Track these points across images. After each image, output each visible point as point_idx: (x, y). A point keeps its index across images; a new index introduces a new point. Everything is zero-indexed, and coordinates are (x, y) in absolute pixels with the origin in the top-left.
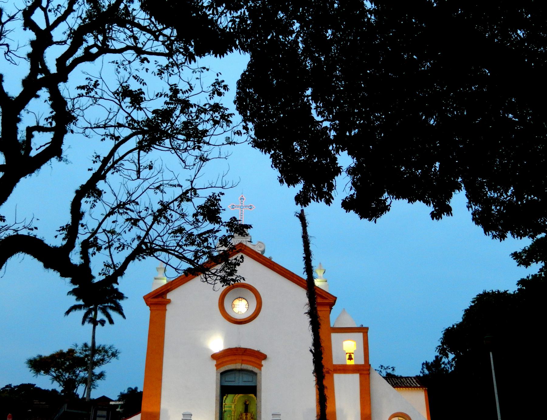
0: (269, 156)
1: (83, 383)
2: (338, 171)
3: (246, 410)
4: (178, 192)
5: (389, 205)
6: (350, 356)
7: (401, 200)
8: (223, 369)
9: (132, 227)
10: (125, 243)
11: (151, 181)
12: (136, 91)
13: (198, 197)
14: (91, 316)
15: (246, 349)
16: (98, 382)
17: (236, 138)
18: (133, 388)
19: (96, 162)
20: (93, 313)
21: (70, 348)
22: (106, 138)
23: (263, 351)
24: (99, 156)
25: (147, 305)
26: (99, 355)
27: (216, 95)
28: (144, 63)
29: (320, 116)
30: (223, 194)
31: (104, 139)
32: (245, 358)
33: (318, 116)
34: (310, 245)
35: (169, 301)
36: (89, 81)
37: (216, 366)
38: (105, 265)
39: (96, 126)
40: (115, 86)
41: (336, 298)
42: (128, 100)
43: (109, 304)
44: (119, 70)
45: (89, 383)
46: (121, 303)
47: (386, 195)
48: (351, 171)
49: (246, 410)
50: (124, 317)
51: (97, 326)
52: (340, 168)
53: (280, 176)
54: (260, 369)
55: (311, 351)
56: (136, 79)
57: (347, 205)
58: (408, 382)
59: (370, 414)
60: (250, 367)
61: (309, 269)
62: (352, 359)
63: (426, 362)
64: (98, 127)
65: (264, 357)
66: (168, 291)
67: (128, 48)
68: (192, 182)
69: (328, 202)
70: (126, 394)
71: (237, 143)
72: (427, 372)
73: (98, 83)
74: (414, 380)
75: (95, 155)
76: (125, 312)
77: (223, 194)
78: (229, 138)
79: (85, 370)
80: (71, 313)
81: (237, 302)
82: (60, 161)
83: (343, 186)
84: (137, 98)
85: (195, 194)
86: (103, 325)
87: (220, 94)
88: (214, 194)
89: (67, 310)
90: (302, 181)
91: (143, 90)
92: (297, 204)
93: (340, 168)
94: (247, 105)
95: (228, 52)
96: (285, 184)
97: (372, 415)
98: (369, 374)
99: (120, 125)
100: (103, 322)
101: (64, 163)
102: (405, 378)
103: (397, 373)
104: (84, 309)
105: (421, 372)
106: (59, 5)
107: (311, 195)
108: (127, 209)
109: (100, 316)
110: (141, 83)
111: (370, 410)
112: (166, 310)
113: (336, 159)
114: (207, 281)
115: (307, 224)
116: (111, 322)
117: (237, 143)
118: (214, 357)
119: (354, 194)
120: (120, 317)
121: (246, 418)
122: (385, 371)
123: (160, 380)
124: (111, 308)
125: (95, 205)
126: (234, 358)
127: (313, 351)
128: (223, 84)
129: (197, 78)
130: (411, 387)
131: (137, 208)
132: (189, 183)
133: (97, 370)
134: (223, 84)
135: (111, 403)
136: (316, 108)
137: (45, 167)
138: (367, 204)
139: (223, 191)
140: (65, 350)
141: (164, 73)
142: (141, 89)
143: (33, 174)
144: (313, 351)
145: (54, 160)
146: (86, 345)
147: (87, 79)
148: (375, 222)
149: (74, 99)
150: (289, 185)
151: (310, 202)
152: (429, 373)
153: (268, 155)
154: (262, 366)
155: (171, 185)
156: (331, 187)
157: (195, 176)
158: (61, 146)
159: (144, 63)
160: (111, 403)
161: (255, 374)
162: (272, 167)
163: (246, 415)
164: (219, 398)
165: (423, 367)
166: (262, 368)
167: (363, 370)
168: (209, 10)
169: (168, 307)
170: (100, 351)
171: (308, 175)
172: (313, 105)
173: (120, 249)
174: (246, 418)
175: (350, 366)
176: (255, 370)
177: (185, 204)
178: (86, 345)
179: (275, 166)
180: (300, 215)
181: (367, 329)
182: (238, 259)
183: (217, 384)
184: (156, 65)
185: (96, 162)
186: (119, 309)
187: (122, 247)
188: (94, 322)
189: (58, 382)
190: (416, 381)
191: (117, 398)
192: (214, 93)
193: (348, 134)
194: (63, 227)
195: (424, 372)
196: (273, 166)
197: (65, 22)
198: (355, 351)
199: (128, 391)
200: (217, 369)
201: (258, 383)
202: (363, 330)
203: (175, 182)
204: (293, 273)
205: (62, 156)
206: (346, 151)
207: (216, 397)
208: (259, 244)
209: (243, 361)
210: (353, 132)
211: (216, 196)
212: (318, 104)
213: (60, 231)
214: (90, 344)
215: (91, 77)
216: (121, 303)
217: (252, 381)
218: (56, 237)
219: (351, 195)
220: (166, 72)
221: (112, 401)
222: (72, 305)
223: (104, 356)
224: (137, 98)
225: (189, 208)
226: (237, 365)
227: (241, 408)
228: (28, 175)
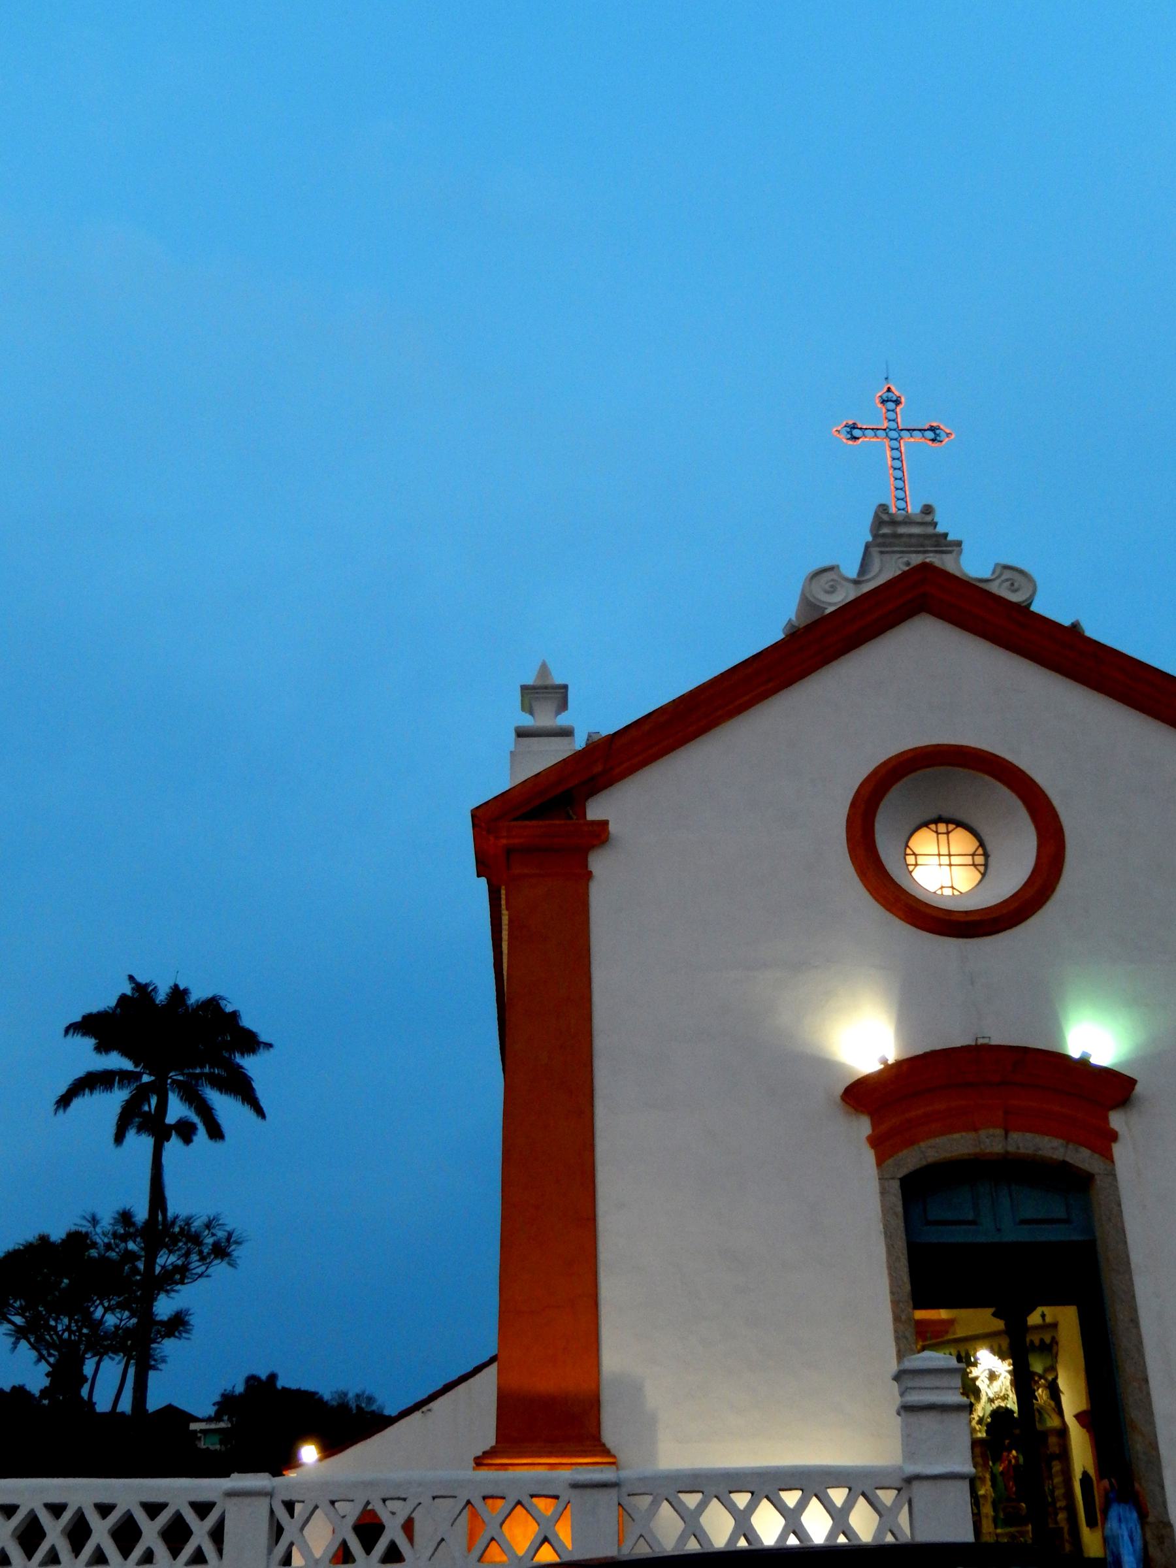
1: (116, 1352)
8: (911, 1159)
16: (168, 1347)
20: (154, 1101)
21: (74, 1228)
26: (171, 1252)
35: (599, 834)
37: (876, 1142)
43: (207, 1070)
45: (139, 1347)
46: (250, 1064)
50: (260, 1112)
51: (168, 1145)
54: (1108, 1156)
60: (1051, 1147)
79: (122, 1306)
80: (77, 1103)
89: (62, 1089)
104: (121, 1087)
109: (177, 1109)
112: (589, 875)
116: (216, 1132)
118: (862, 1095)
120: (247, 1112)
123: (585, 1220)
133: (164, 1307)
135: (194, 1426)
140: (57, 1234)
146: (125, 1217)
154: (1114, 1136)
160: (194, 1426)
166: (1117, 1149)
169: (600, 864)
170: (175, 1239)
176: (1083, 1158)
178: (125, 1217)
183: (888, 1235)
186: (242, 1088)
188: (159, 1131)
189: (33, 1347)
191: (211, 1411)
200: (880, 1162)
208: (1007, 574)
214: (141, 1214)
216: (250, 1064)
217: (1067, 1221)
221: (196, 1420)
222: (80, 1073)
223: (187, 1254)
226: (983, 1133)
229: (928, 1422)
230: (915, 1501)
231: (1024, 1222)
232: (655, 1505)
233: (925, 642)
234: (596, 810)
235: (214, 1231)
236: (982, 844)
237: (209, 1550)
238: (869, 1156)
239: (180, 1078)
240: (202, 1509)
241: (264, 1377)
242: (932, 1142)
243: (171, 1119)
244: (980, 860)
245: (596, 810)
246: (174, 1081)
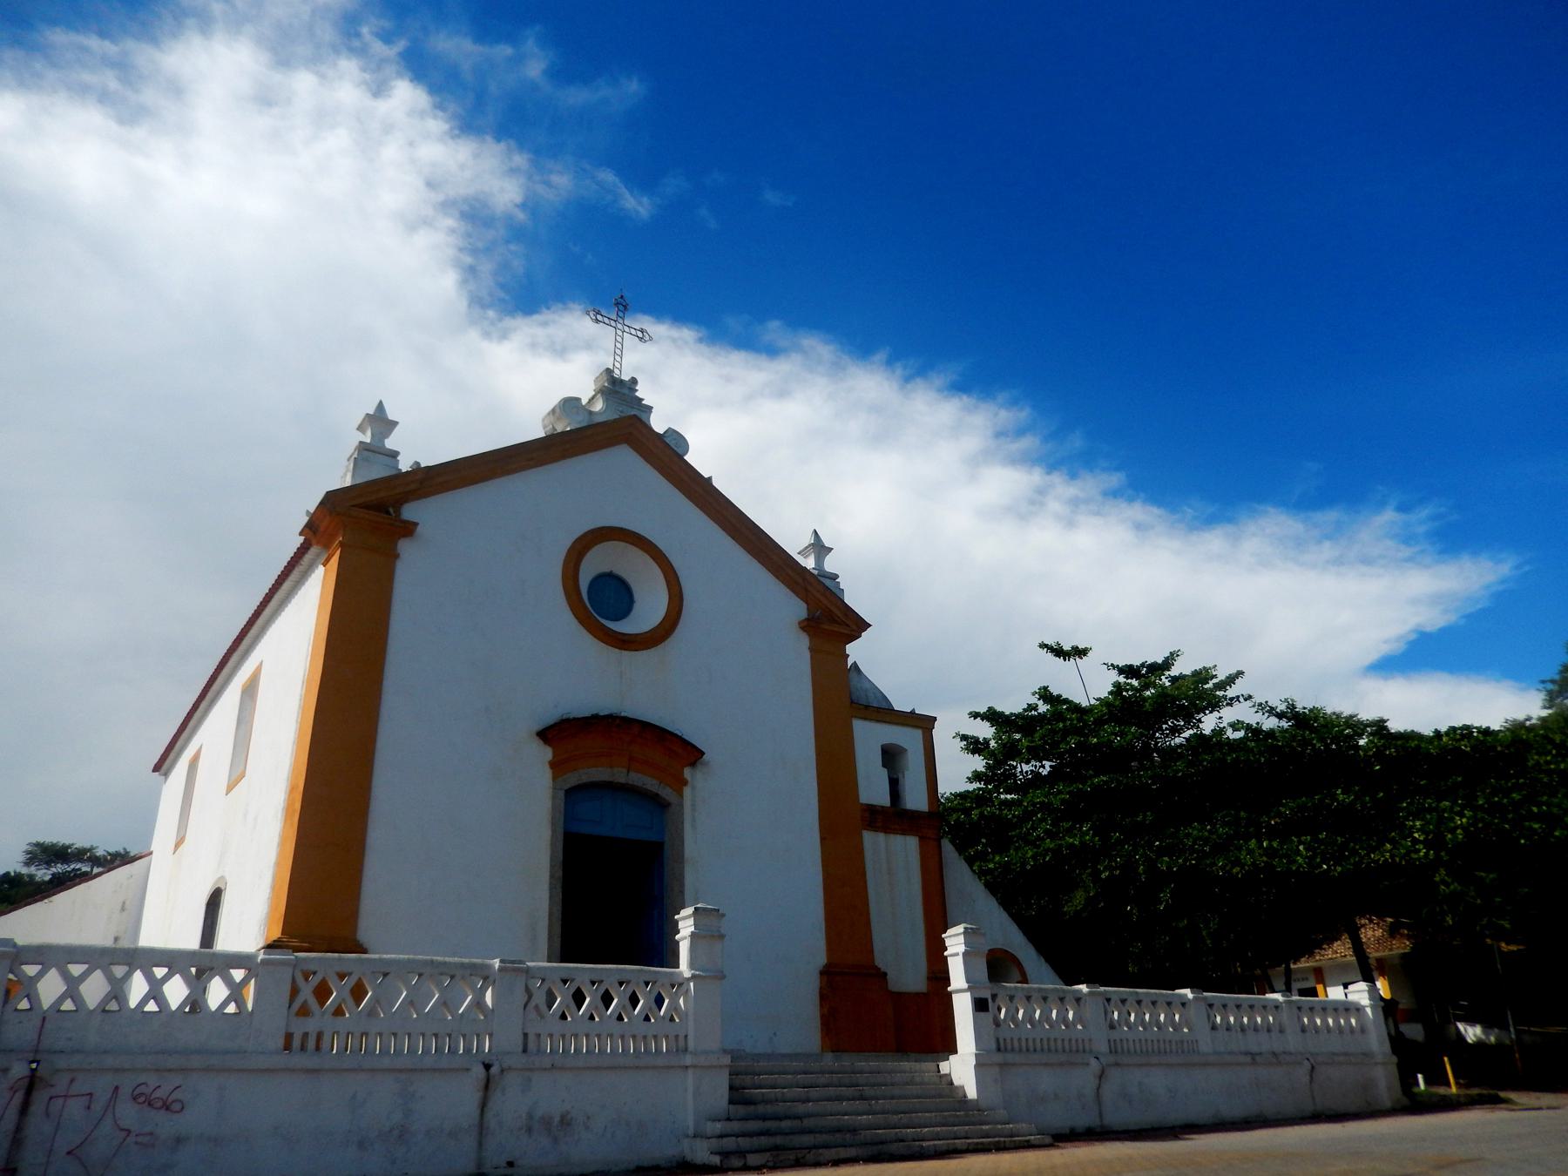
8: (573, 779)
35: (409, 529)
37: (555, 765)
112: (397, 556)
169: (405, 547)
176: (666, 793)
183: (553, 824)
200: (554, 778)
233: (623, 458)
234: (410, 512)
238: (547, 774)
245: (410, 512)
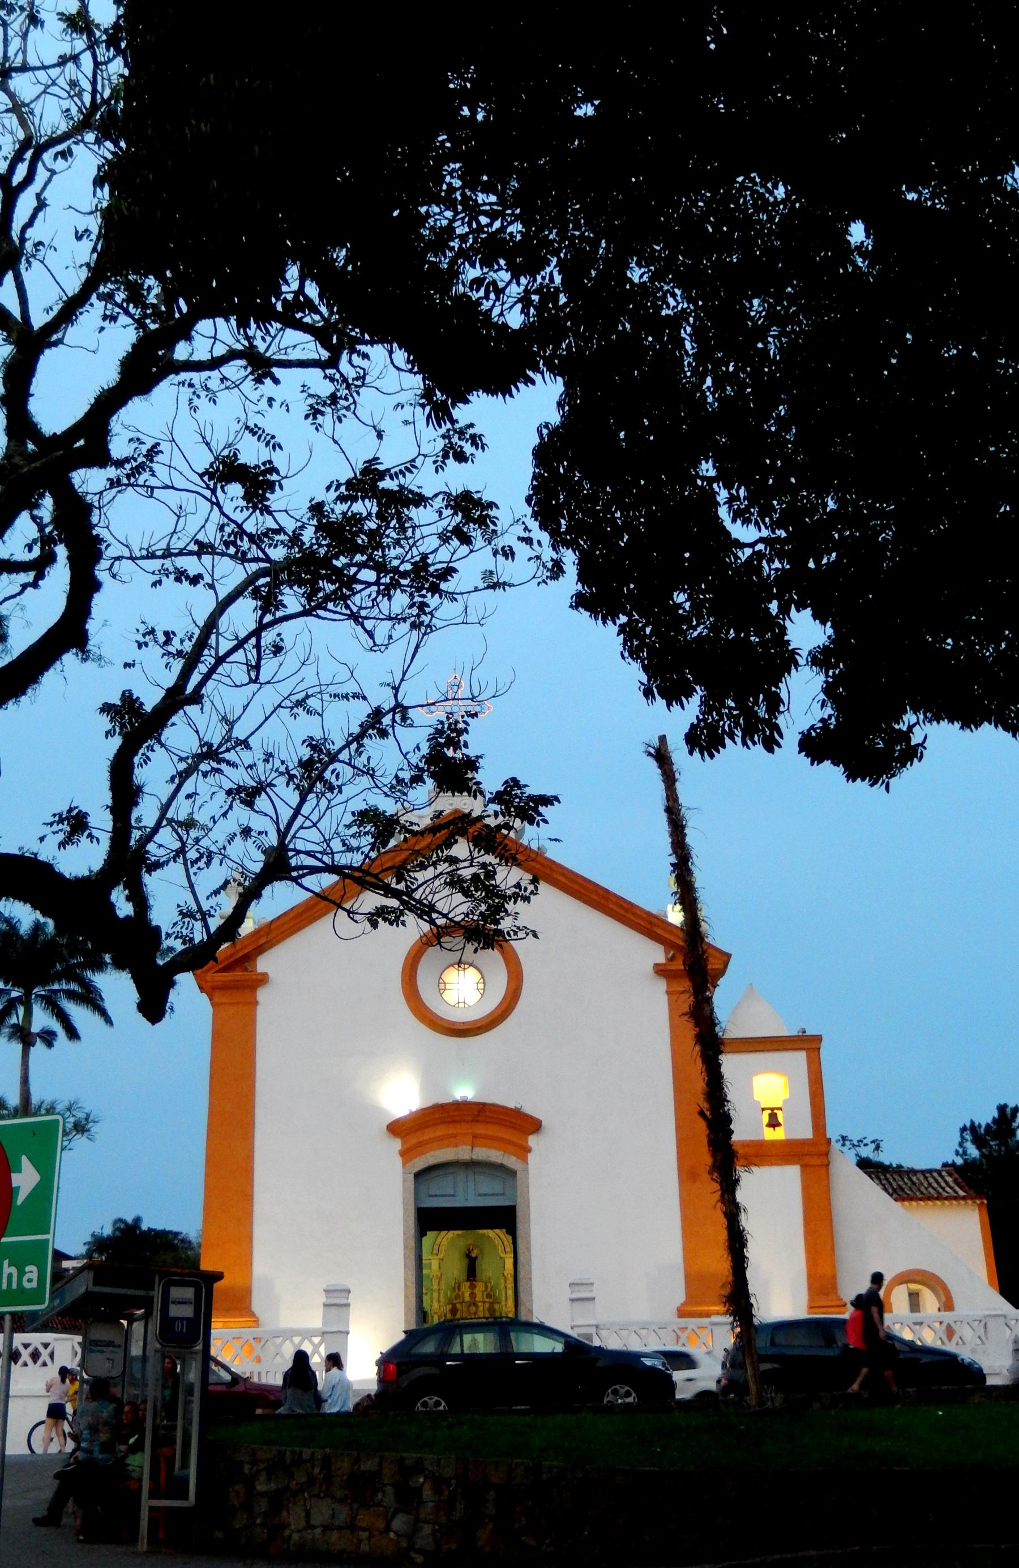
0: (616, 629)
2: (787, 660)
3: (472, 1272)
4: (360, 712)
5: (922, 745)
6: (773, 1116)
7: (944, 724)
8: (420, 1163)
9: (231, 807)
10: (213, 849)
11: (285, 688)
12: (257, 466)
13: (411, 726)
14: (14, 1020)
15: (484, 1104)
17: (506, 571)
18: (129, 1220)
19: (146, 644)
20: (21, 1010)
22: (164, 579)
23: (528, 1109)
24: (152, 632)
25: (202, 989)
27: (451, 461)
28: (263, 383)
29: (739, 522)
30: (474, 715)
31: (160, 582)
32: (481, 1129)
33: (734, 521)
34: (687, 831)
35: (263, 980)
36: (136, 445)
37: (403, 1153)
38: (181, 913)
39: (144, 553)
40: (203, 460)
41: (728, 956)
42: (236, 489)
43: (65, 987)
44: (196, 402)
47: (910, 718)
48: (820, 659)
49: (472, 1272)
50: (108, 1021)
52: (794, 652)
53: (644, 679)
54: (525, 1160)
55: (701, 1113)
56: (254, 434)
57: (816, 746)
58: (930, 1185)
59: (834, 1277)
61: (687, 895)
62: (779, 1125)
63: (972, 1123)
64: (151, 556)
65: (534, 1126)
66: (261, 950)
67: (232, 355)
68: (396, 689)
69: (770, 745)
70: (109, 1238)
71: (510, 585)
72: (973, 1152)
73: (159, 448)
74: (949, 1179)
75: (143, 629)
76: (108, 1005)
77: (474, 715)
78: (491, 572)
81: (452, 975)
82: (84, 660)
83: (804, 698)
84: (258, 484)
85: (404, 718)
86: (50, 1045)
87: (461, 457)
88: (449, 715)
90: (698, 688)
91: (276, 464)
92: (691, 753)
93: (794, 652)
94: (560, 507)
95: (521, 386)
96: (660, 702)
97: (839, 1275)
98: (827, 1165)
99: (204, 548)
100: (48, 1037)
101: (95, 665)
102: (923, 1172)
103: (887, 1157)
105: (957, 1153)
106: (40, 243)
107: (726, 728)
108: (224, 760)
109: (41, 1019)
110: (267, 444)
111: (833, 1266)
112: (256, 1003)
113: (783, 630)
114: (439, 943)
115: (677, 776)
116: (73, 1033)
117: (510, 585)
118: (396, 1128)
119: (830, 716)
120: (97, 1019)
121: (473, 1295)
122: (853, 1152)
123: (247, 1197)
124: (71, 995)
125: (148, 758)
126: (451, 1130)
127: (708, 1113)
128: (471, 431)
129: (406, 422)
130: (939, 1197)
131: (247, 757)
132: (390, 693)
134: (471, 431)
136: (731, 500)
137: (50, 678)
138: (863, 745)
139: (474, 708)
141: (322, 413)
142: (270, 462)
143: (23, 698)
144: (708, 1113)
145: (70, 659)
147: (131, 440)
148: (887, 789)
149: (101, 493)
150: (669, 705)
151: (724, 747)
152: (982, 1155)
153: (612, 629)
154: (529, 1150)
155: (335, 696)
156: (775, 703)
157: (404, 674)
158: (85, 622)
159: (263, 383)
161: (513, 1173)
162: (623, 657)
163: (473, 1287)
164: (412, 1244)
165: (962, 1137)
167: (811, 1156)
168: (477, 291)
169: (263, 995)
171: (710, 668)
172: (723, 495)
173: (201, 864)
174: (473, 1295)
175: (774, 1144)
176: (511, 1161)
177: (373, 745)
179: (631, 655)
180: (658, 750)
181: (818, 1039)
182: (523, 885)
183: (405, 1203)
184: (305, 395)
185: (146, 644)
187: (204, 859)
190: (955, 1181)
191: (83, 1250)
192: (446, 456)
193: (811, 565)
194: (60, 815)
195: (965, 1153)
196: (626, 654)
197: (70, 294)
198: (785, 1102)
199: (116, 1229)
200: (404, 1164)
201: (519, 1200)
202: (808, 1043)
203: (351, 688)
204: (607, 891)
205: (89, 647)
206: (808, 611)
207: (406, 1239)
209: (476, 1140)
210: (825, 561)
211: (457, 722)
212: (734, 492)
213: (51, 824)
215: (141, 436)
217: (503, 1194)
218: (42, 839)
219: (822, 720)
220: (328, 410)
221: (68, 1258)
224: (258, 484)
225: (386, 756)
226: (460, 1148)
227: (456, 1269)
228: (10, 703)
229: (334, 1310)
230: (988, 1325)
231: (480, 1195)
232: (284, 1341)
235: (74, 1113)
236: (483, 977)
237: (48, 1361)
239: (43, 993)
240: (46, 1346)
241: (130, 1220)
242: (432, 1153)
243: (35, 1028)
244: (481, 986)
246: (37, 996)
